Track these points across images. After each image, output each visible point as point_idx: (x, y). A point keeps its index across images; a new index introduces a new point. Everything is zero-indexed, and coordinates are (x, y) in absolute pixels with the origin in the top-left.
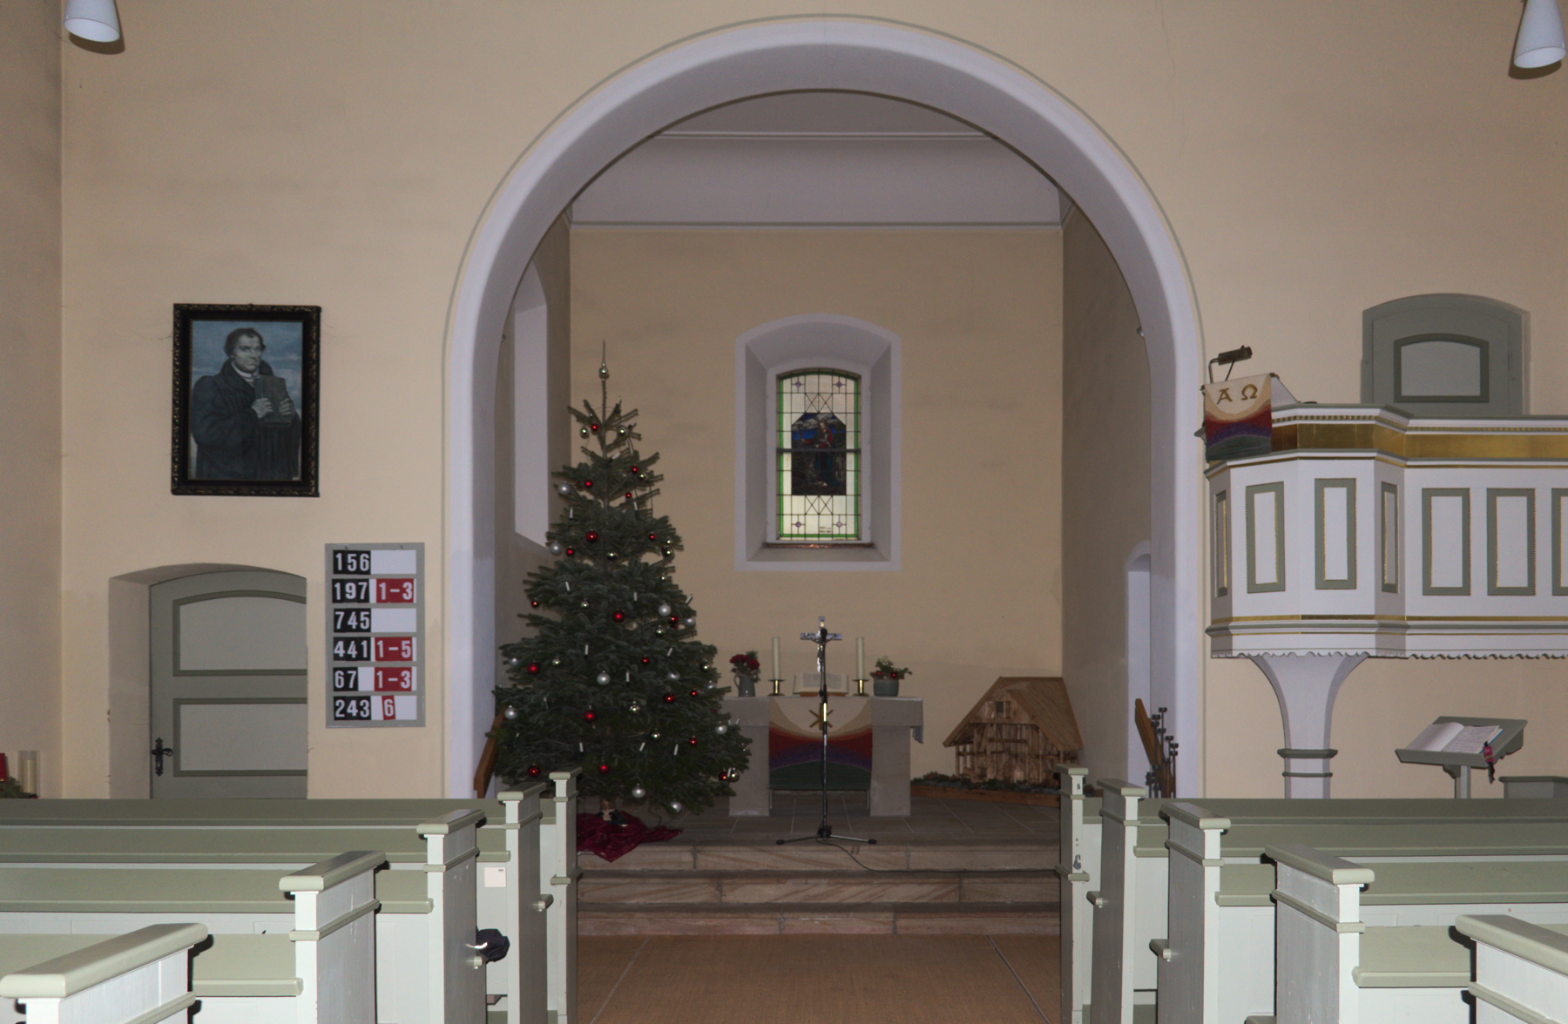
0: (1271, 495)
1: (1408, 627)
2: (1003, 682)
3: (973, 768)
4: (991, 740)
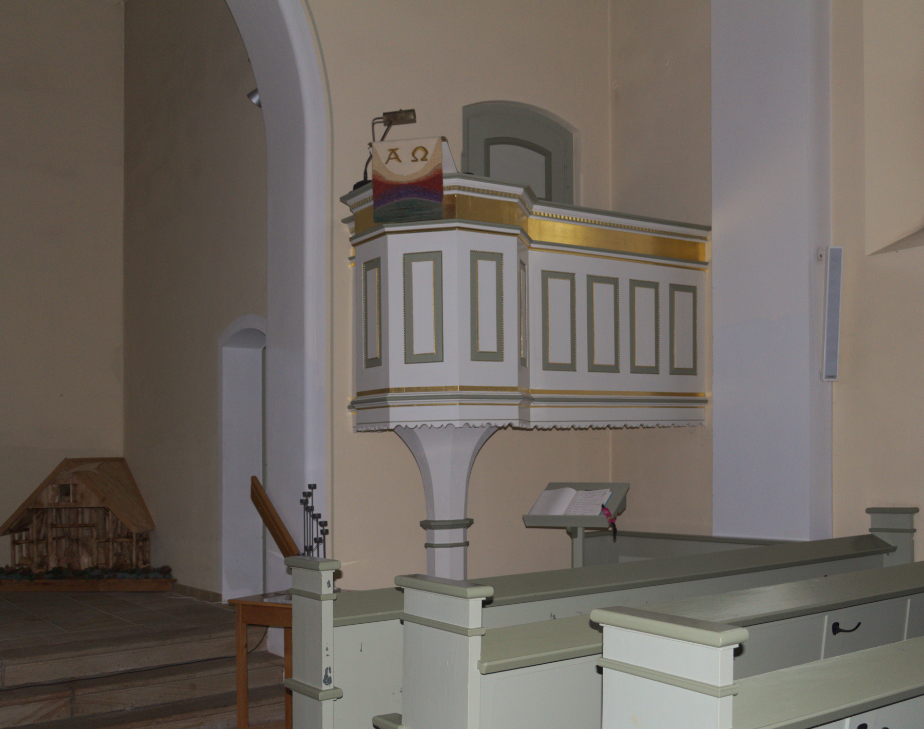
0: (429, 265)
1: (533, 400)
2: (68, 464)
3: (29, 557)
4: (53, 526)
